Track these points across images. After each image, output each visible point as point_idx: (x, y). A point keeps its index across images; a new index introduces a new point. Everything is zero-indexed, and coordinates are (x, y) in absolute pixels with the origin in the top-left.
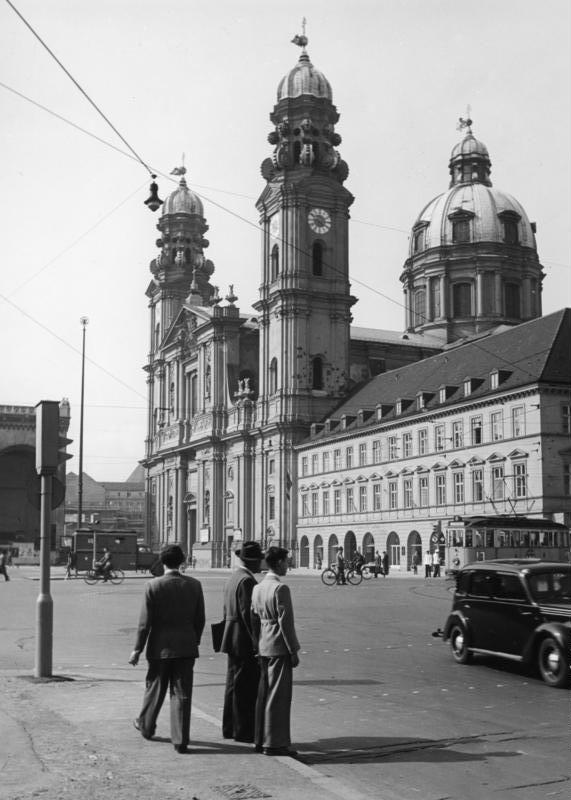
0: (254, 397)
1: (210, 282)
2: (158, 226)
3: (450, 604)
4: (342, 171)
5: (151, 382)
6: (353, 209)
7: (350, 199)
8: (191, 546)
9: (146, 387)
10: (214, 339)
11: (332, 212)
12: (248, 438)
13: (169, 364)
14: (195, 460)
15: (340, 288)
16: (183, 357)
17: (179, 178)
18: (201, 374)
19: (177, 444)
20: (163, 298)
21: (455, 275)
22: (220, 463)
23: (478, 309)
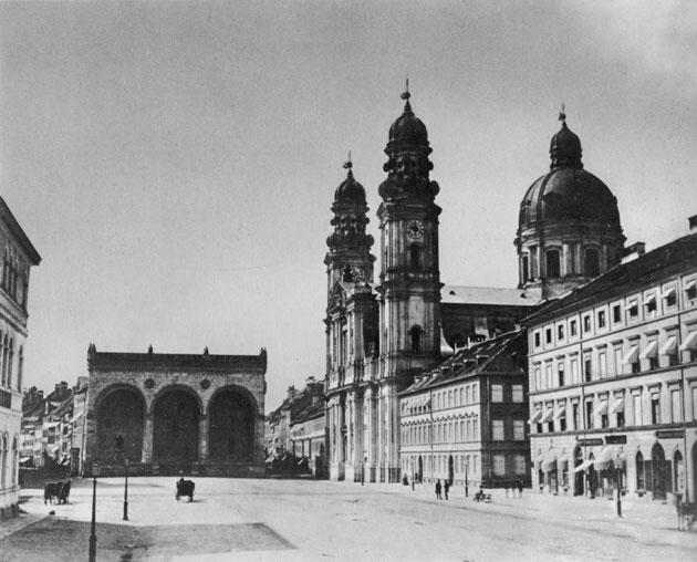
0: (377, 355)
1: (371, 252)
2: (385, 151)
3: (398, 484)
4: (434, 188)
5: (328, 332)
6: (441, 218)
7: (439, 210)
8: (447, 491)
9: (325, 335)
10: (354, 310)
11: (426, 220)
12: (375, 387)
13: (350, 313)
14: (667, 354)
15: (10, 511)
16: (341, 319)
17: (347, 170)
18: (348, 334)
19: (336, 386)
20: (390, 222)
21: (548, 244)
22: (342, 403)
23: (564, 271)
